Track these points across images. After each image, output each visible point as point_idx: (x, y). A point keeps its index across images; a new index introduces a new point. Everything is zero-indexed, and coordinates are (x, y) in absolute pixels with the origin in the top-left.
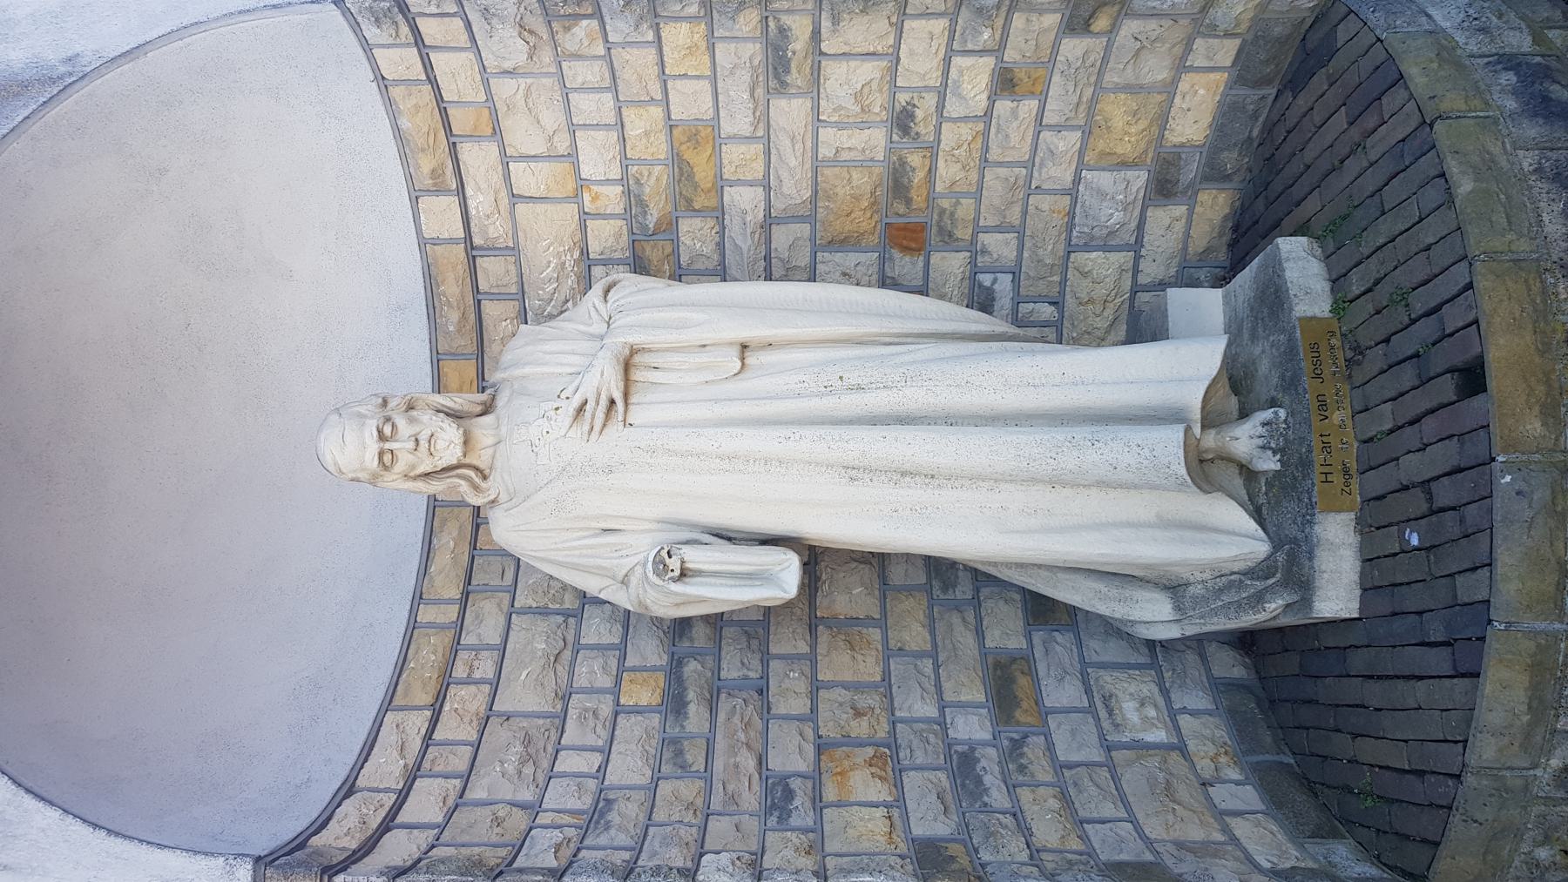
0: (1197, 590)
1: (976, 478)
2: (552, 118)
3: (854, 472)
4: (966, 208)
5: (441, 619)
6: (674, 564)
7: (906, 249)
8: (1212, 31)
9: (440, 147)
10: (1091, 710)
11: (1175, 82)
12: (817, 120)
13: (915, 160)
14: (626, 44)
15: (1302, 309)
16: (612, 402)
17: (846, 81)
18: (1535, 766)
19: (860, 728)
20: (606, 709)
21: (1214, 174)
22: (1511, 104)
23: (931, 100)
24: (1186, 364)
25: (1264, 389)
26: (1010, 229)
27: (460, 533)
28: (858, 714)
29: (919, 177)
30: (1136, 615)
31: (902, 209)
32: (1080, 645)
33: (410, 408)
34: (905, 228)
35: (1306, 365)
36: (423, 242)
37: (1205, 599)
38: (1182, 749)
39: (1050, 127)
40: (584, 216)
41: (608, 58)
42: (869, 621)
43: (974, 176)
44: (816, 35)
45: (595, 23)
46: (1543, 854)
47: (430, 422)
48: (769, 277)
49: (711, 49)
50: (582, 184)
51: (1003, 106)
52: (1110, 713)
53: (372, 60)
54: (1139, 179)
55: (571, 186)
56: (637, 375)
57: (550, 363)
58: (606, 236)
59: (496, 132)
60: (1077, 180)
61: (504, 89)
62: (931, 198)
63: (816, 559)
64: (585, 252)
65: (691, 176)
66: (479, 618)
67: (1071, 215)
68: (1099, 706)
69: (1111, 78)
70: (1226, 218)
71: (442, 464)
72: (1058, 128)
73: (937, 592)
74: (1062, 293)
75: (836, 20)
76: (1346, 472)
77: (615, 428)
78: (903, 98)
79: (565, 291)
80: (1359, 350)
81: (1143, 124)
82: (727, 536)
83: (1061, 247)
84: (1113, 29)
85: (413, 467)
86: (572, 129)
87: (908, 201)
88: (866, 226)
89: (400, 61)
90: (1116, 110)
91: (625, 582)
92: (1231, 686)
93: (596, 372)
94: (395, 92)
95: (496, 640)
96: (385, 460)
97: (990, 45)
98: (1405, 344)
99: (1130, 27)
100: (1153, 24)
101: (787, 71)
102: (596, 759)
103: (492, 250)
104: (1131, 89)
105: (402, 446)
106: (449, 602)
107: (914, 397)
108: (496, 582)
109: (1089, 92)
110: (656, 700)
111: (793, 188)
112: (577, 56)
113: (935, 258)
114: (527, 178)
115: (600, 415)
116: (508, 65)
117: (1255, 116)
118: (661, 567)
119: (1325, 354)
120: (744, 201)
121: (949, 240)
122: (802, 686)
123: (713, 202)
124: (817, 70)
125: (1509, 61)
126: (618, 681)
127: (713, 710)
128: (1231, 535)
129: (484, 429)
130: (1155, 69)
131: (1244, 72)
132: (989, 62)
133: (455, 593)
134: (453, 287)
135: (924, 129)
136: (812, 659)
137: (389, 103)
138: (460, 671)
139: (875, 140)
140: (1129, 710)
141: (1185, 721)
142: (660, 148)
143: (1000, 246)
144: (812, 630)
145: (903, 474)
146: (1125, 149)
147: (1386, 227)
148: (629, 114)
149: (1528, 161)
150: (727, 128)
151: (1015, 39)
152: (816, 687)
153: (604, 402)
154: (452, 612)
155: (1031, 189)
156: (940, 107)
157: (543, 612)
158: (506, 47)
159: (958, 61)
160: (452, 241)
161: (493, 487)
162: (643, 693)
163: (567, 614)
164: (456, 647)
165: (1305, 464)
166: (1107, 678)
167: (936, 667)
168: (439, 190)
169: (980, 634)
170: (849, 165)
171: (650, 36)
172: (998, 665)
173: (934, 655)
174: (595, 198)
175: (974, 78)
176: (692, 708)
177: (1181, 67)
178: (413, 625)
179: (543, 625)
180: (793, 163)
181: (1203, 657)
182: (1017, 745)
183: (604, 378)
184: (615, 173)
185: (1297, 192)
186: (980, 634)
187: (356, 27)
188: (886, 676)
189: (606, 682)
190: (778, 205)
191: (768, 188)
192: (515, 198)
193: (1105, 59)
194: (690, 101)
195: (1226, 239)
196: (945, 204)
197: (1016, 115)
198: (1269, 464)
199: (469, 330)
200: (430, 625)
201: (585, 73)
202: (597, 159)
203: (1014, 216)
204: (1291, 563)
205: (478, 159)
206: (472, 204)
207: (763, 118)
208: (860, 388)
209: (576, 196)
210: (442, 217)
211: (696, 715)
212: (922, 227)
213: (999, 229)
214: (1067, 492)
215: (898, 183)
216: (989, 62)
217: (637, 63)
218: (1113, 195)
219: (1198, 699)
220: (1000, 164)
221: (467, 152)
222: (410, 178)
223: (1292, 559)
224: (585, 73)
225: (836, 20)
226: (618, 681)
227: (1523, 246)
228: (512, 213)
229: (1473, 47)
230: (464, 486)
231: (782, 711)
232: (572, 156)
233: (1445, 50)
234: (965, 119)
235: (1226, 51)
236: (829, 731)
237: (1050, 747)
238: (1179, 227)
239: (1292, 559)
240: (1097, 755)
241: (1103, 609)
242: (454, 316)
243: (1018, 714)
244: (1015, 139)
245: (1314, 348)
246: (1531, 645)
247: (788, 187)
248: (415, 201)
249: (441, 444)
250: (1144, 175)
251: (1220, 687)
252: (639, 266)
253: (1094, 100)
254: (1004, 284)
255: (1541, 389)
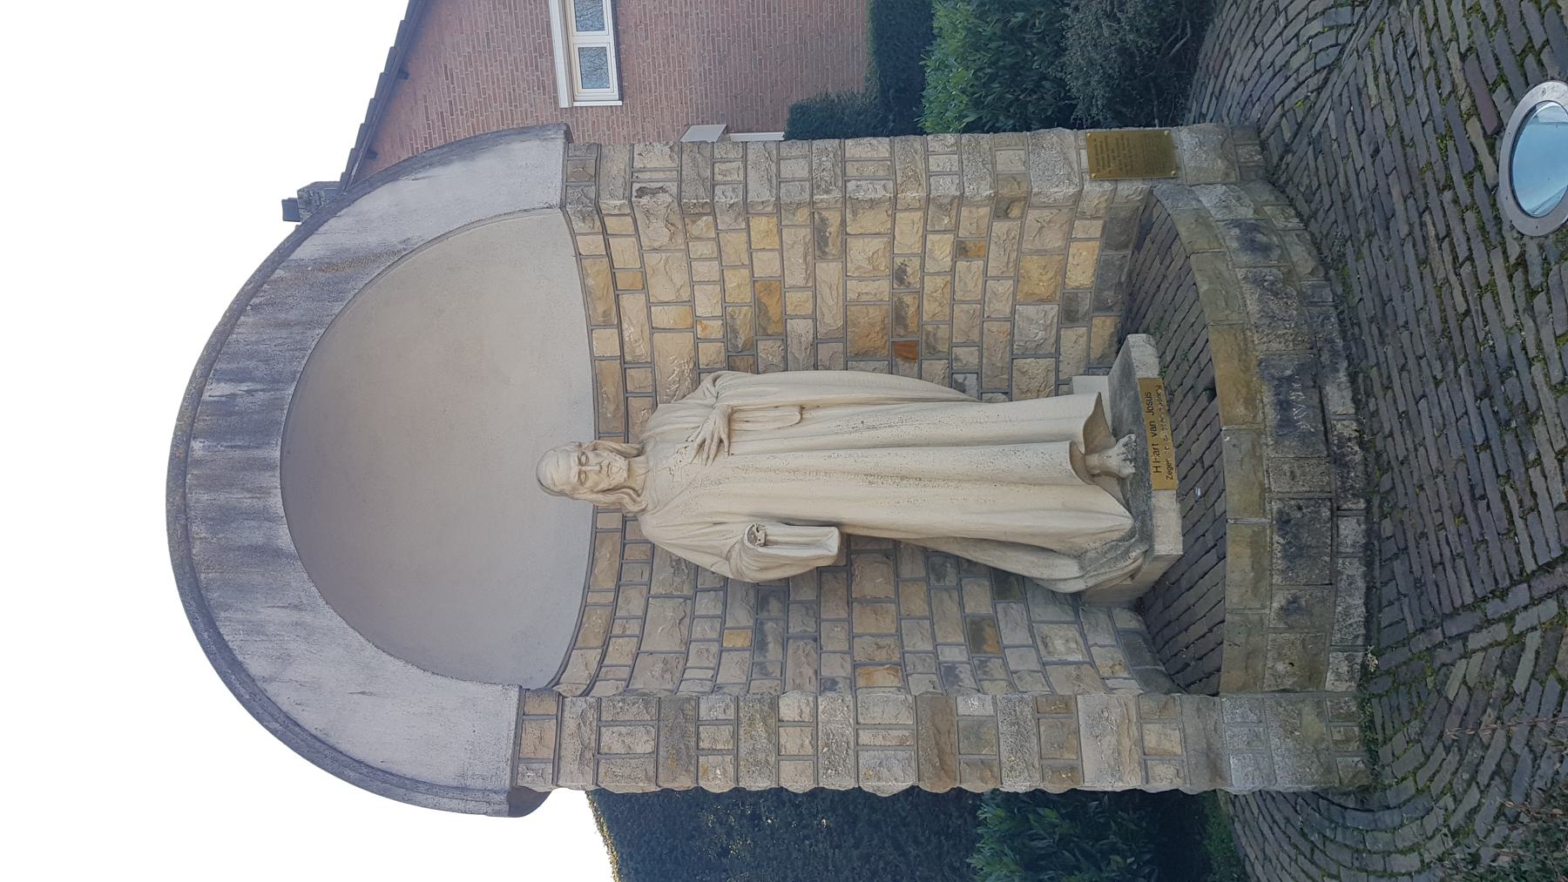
0: (1092, 554)
1: (947, 479)
2: (680, 278)
3: (872, 477)
4: (943, 331)
5: (603, 601)
6: (760, 535)
7: (906, 359)
8: (1083, 216)
9: (607, 300)
10: (1035, 646)
11: (1067, 247)
12: (846, 275)
13: (908, 300)
14: (727, 231)
15: (1140, 374)
16: (721, 441)
17: (862, 251)
18: (1264, 607)
19: (881, 656)
20: (714, 648)
21: (1101, 307)
22: (1235, 245)
23: (916, 262)
24: (1071, 412)
25: (1125, 428)
26: (973, 344)
27: (620, 538)
28: (879, 647)
29: (912, 310)
30: (1057, 574)
31: (902, 332)
32: (1028, 611)
33: (595, 449)
34: (905, 344)
35: (1144, 406)
36: (594, 359)
37: (1097, 559)
38: (1092, 664)
39: (993, 278)
41: (717, 240)
42: (888, 600)
43: (947, 310)
44: (843, 222)
45: (711, 218)
46: (1280, 667)
47: (607, 457)
48: (816, 368)
49: (780, 232)
50: (697, 319)
51: (962, 265)
52: (1046, 646)
53: (575, 243)
54: (1053, 310)
55: (690, 321)
56: (736, 426)
57: (683, 421)
58: (711, 352)
59: (645, 288)
60: (1013, 312)
61: (652, 259)
62: (920, 326)
64: (696, 364)
65: (766, 312)
66: (628, 601)
67: (1012, 334)
68: (1038, 642)
69: (1026, 246)
70: (1112, 335)
71: (614, 483)
72: (997, 278)
73: (933, 581)
74: (1010, 386)
75: (855, 213)
76: (1169, 466)
77: (723, 457)
78: (898, 261)
79: (684, 389)
80: (1172, 393)
81: (1050, 275)
82: (789, 522)
83: (1007, 357)
84: (1023, 216)
85: (597, 484)
86: (692, 284)
87: (906, 327)
88: (879, 343)
89: (592, 244)
90: (1032, 266)
91: (727, 559)
92: (1127, 632)
93: (711, 422)
94: (586, 262)
95: (640, 613)
96: (582, 477)
97: (950, 227)
98: (1188, 383)
99: (1033, 215)
100: (1046, 212)
101: (826, 245)
102: (711, 673)
103: (637, 364)
104: (1041, 252)
105: (592, 468)
106: (608, 591)
107: (908, 431)
108: (637, 579)
109: (1014, 255)
110: (747, 643)
111: (832, 319)
112: (698, 238)
113: (925, 364)
114: (662, 316)
115: (714, 447)
116: (656, 245)
117: (1121, 268)
118: (752, 538)
119: (1154, 398)
120: (800, 328)
121: (933, 352)
122: (843, 636)
123: (780, 330)
124: (845, 244)
125: (1237, 223)
126: (721, 635)
127: (784, 648)
128: (1106, 514)
130: (1053, 240)
131: (1109, 240)
132: (950, 237)
133: (612, 585)
134: (611, 389)
135: (913, 280)
136: (851, 623)
137: (581, 269)
138: (617, 631)
139: (883, 287)
140: (1059, 644)
141: (1094, 650)
142: (747, 296)
143: (968, 356)
144: (849, 603)
145: (902, 478)
146: (1042, 290)
147: (1179, 316)
148: (728, 274)
149: (1240, 273)
150: (789, 282)
151: (964, 223)
152: (852, 637)
153: (716, 440)
154: (611, 596)
155: (984, 318)
156: (923, 266)
157: (669, 596)
158: (657, 232)
159: (930, 237)
160: (612, 358)
161: (645, 500)
162: (741, 640)
163: (686, 598)
165: (1146, 463)
166: (1045, 629)
167: (932, 625)
168: (606, 325)
169: (961, 605)
170: (867, 304)
171: (743, 225)
172: (973, 623)
173: (931, 619)
174: (704, 329)
175: (942, 248)
176: (771, 646)
177: (1069, 239)
178: (584, 606)
179: (670, 603)
180: (831, 303)
181: (1110, 617)
182: (983, 664)
183: (714, 425)
184: (718, 312)
185: (1143, 311)
186: (961, 605)
187: (569, 222)
188: (899, 629)
189: (715, 635)
190: (822, 330)
191: (815, 320)
192: (654, 329)
193: (1021, 235)
194: (766, 265)
196: (929, 328)
197: (970, 270)
198: (1129, 470)
199: (622, 409)
200: (595, 604)
201: (702, 249)
202: (707, 305)
203: (975, 335)
204: (1143, 532)
205: (632, 305)
206: (626, 334)
207: (811, 275)
208: (874, 428)
209: (693, 328)
211: (773, 650)
212: (916, 344)
213: (964, 345)
214: (1005, 488)
215: (899, 317)
216: (950, 237)
217: (735, 243)
218: (1037, 321)
219: (1106, 639)
220: (964, 302)
221: (626, 301)
222: (588, 317)
223: (1143, 522)
224: (702, 249)
225: (855, 213)
226: (721, 635)
227: (1235, 317)
228: (651, 340)
229: (1219, 217)
230: (626, 499)
231: (830, 648)
232: (691, 302)
233: (1202, 218)
234: (938, 273)
235: (1095, 228)
236: (860, 657)
237: (1005, 664)
238: (1083, 341)
239: (1143, 522)
240: (1036, 667)
241: (1034, 573)
242: (612, 407)
243: (985, 647)
244: (971, 285)
245: (1148, 395)
246: (1249, 532)
247: (828, 319)
248: (590, 332)
249: (615, 470)
250: (1056, 308)
251: (1120, 634)
252: (731, 368)
253: (1018, 260)
254: (971, 380)
255: (1244, 391)
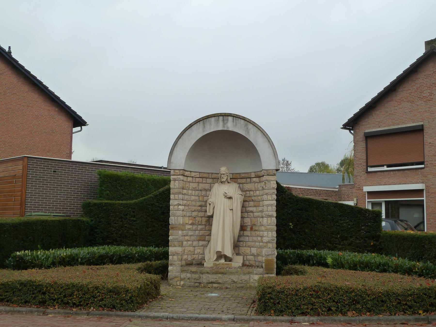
20: (199, 195)
36: (251, 173)
38: (194, 254)
40: (253, 191)
63: (212, 216)
129: (226, 183)
138: (204, 179)
141: (197, 256)
152: (202, 217)
164: (207, 178)
178: (209, 173)
183: (229, 195)
195: (340, 317)
210: (253, 175)
